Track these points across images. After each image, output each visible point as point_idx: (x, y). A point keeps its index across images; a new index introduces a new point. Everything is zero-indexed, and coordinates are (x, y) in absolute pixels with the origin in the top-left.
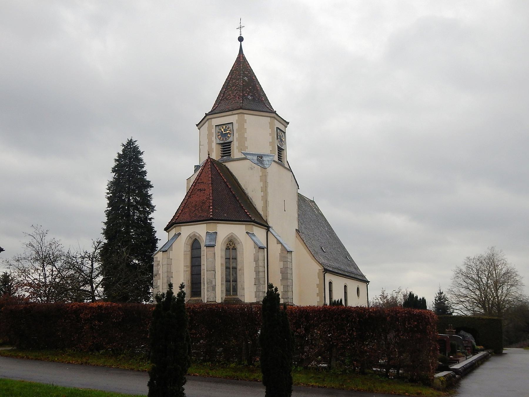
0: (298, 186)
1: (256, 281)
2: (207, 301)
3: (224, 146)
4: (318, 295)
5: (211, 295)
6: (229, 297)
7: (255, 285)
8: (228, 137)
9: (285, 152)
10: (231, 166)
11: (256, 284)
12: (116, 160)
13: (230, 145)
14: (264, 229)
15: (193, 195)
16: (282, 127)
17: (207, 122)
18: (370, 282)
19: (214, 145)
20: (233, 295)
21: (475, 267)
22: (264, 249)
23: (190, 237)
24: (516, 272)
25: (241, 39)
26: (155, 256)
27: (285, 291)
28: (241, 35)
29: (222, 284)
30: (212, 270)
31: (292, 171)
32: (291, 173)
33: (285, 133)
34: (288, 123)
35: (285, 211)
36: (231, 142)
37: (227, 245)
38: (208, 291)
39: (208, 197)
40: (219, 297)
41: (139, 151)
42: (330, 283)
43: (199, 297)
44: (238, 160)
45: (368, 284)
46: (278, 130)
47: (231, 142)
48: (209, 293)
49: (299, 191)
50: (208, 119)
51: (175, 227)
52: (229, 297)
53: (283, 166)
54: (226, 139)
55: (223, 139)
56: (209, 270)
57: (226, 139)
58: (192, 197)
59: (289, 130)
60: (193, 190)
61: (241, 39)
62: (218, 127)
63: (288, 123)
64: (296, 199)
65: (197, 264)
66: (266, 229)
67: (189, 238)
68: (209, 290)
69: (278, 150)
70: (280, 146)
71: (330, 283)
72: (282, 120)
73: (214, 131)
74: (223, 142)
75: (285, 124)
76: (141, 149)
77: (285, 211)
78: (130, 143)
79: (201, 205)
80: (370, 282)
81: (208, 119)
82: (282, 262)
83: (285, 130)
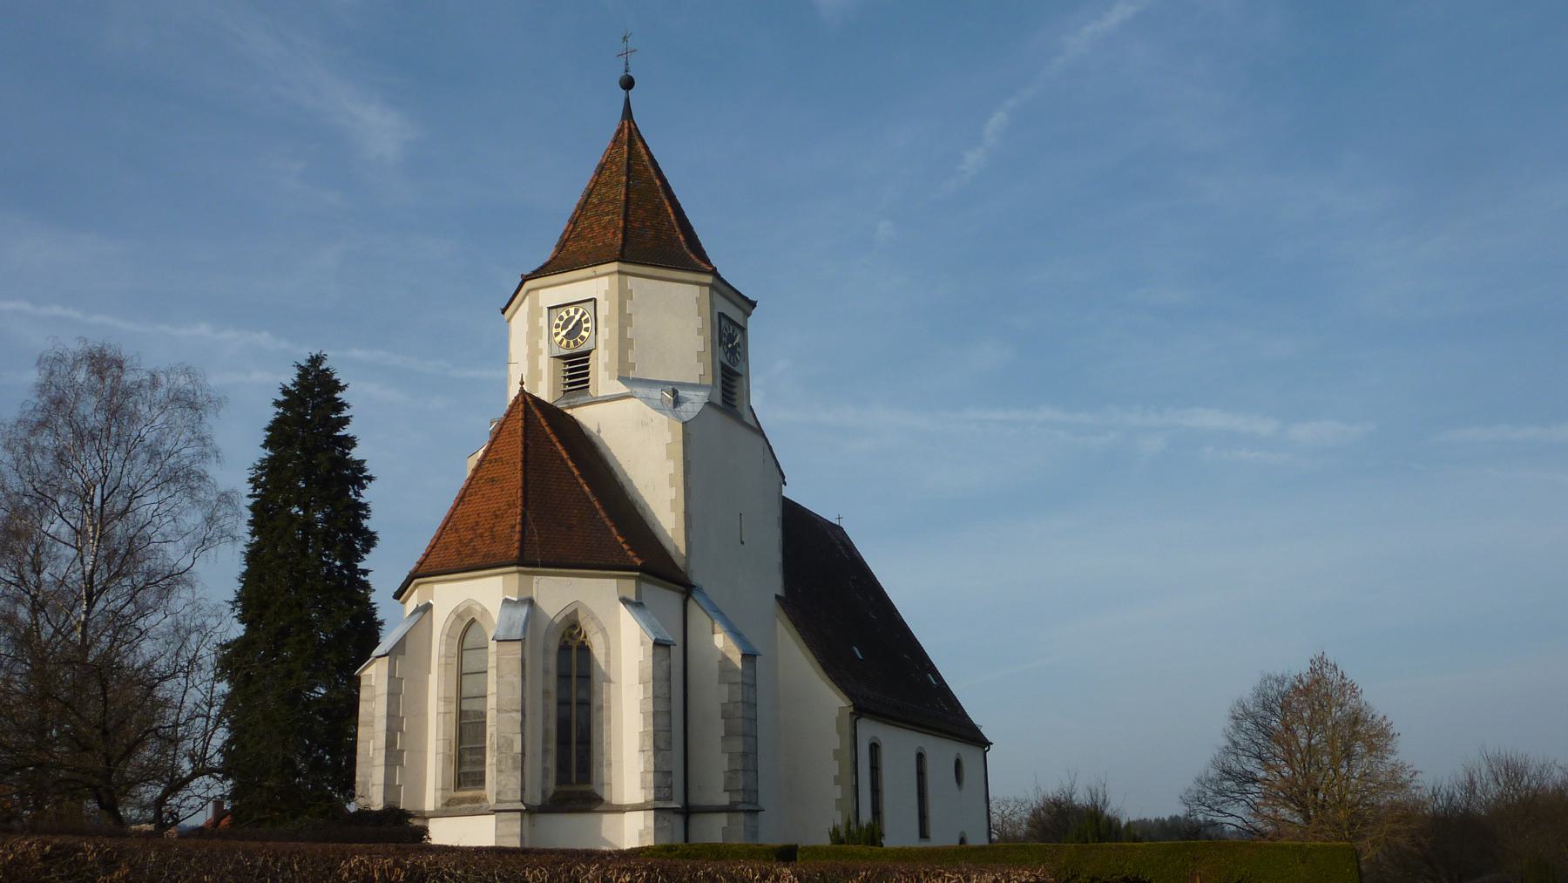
0: (784, 477)
1: (644, 740)
2: (497, 799)
3: (570, 364)
4: (837, 781)
5: (506, 784)
6: (566, 788)
7: (644, 751)
8: (582, 338)
9: (745, 383)
10: (586, 416)
11: (645, 749)
12: (277, 404)
13: (587, 360)
14: (674, 590)
15: (471, 495)
16: (735, 314)
17: (527, 297)
18: (992, 744)
19: (544, 362)
20: (579, 782)
21: (129, 447)
22: (669, 646)
23: (459, 615)
24: (153, 661)
25: (628, 84)
26: (366, 672)
27: (735, 770)
28: (627, 71)
29: (545, 751)
30: (514, 708)
31: (763, 435)
32: (763, 439)
33: (743, 329)
34: (753, 304)
35: (742, 543)
36: (588, 353)
37: (563, 636)
38: (500, 771)
39: (511, 499)
40: (377, 802)
41: (337, 382)
42: (874, 748)
43: (481, 789)
44: (607, 401)
45: (986, 749)
46: (724, 322)
47: (588, 353)
48: (502, 777)
49: (789, 492)
50: (528, 291)
51: (417, 585)
52: (566, 788)
53: (738, 418)
54: (576, 343)
55: (568, 344)
56: (505, 708)
57: (576, 343)
58: (469, 500)
59: (754, 324)
60: (473, 483)
61: (628, 84)
62: (554, 310)
63: (753, 304)
64: (776, 512)
65: (475, 692)
66: (682, 593)
67: (454, 616)
68: (503, 767)
69: (723, 375)
70: (728, 364)
71: (874, 748)
72: (733, 293)
73: (543, 321)
74: (567, 352)
75: (746, 306)
76: (340, 376)
77: (742, 543)
78: (316, 361)
79: (492, 522)
80: (992, 744)
81: (528, 291)
82: (727, 685)
83: (746, 322)
